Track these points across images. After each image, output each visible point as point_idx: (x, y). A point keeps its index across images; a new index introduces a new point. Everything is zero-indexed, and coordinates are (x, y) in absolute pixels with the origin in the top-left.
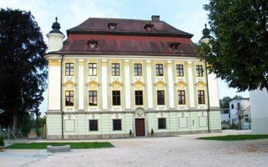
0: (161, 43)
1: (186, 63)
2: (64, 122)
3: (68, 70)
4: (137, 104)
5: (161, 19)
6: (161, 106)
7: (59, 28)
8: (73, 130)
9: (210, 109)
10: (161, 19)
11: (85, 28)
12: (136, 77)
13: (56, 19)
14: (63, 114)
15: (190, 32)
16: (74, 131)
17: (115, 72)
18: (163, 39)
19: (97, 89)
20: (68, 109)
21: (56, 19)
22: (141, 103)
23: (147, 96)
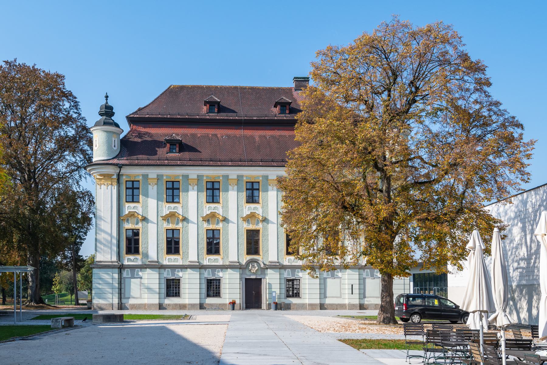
2: (122, 280)
6: (172, 257)
7: (113, 114)
8: (339, 296)
11: (157, 113)
12: (168, 205)
13: (107, 97)
14: (121, 268)
20: (129, 260)
22: (257, 252)
23: (147, 238)
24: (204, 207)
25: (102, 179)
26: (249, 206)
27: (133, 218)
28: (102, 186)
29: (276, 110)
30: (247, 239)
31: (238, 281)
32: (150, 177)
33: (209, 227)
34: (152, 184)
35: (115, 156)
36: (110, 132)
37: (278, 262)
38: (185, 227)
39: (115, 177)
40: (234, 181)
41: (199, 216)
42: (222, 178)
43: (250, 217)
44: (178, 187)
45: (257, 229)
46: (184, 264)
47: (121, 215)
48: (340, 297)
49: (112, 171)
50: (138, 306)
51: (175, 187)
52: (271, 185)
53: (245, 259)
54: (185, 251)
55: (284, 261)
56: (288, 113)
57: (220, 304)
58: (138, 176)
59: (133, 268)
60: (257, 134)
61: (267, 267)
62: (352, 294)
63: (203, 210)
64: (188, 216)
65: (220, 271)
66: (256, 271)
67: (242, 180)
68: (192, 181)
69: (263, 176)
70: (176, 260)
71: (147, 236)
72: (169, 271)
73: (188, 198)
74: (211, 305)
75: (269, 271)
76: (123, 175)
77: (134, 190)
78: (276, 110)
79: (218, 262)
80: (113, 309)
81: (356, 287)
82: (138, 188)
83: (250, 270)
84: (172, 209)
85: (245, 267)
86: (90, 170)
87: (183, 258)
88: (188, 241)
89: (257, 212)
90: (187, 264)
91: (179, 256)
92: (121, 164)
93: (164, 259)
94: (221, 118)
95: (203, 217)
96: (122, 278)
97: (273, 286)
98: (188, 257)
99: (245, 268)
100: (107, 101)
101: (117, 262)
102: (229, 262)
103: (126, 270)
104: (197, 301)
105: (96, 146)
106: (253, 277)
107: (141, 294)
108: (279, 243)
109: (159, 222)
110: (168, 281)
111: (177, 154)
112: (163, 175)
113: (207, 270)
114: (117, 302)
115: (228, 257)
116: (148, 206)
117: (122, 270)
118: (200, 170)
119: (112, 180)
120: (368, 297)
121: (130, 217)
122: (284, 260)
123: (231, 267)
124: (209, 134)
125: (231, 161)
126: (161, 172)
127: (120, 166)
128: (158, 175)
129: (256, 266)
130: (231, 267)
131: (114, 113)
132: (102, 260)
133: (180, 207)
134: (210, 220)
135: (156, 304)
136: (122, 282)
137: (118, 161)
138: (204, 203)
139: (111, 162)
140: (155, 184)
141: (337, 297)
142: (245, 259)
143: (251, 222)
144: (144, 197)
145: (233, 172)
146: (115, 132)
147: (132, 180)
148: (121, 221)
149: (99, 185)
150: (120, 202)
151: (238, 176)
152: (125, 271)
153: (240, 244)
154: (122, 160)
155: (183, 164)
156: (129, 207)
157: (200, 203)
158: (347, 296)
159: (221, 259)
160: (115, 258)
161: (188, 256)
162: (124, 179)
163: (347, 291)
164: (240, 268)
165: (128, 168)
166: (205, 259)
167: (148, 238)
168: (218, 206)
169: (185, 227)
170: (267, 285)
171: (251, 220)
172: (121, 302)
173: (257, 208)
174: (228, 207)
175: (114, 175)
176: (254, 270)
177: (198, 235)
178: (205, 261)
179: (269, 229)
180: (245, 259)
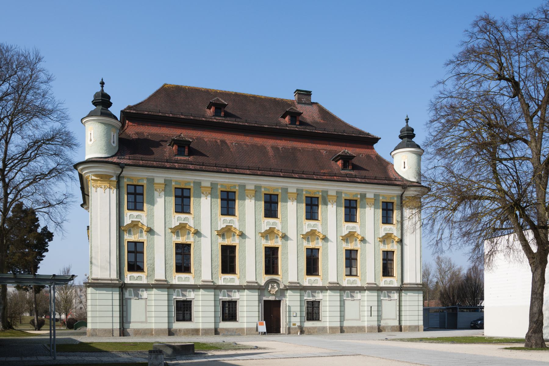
0: (272, 147)
1: (151, 181)
2: (124, 301)
4: (267, 272)
5: (313, 99)
6: (228, 276)
7: (110, 104)
10: (313, 99)
13: (102, 84)
14: (122, 287)
15: (374, 133)
16: (146, 322)
17: (135, 201)
18: (324, 148)
19: (144, 238)
21: (102, 84)
24: (219, 220)
25: (98, 180)
26: (267, 221)
27: (136, 229)
28: (99, 189)
29: (210, 112)
30: (190, 255)
31: (256, 303)
32: (247, 187)
33: (224, 242)
34: (158, 190)
35: (114, 154)
36: (109, 124)
37: (257, 283)
38: (197, 241)
39: (114, 179)
40: (251, 192)
41: (213, 230)
42: (238, 188)
43: (269, 233)
44: (141, 192)
45: (188, 243)
46: (196, 283)
47: (121, 225)
48: (360, 320)
49: (110, 171)
50: (143, 332)
51: (137, 192)
52: (291, 198)
53: (263, 279)
54: (198, 269)
55: (305, 281)
56: (298, 124)
57: (237, 329)
58: (142, 179)
59: (137, 287)
60: (269, 143)
61: (286, 289)
62: (371, 316)
63: (217, 223)
64: (201, 229)
65: (320, 292)
66: (277, 292)
67: (260, 192)
68: (292, 195)
69: (282, 189)
70: (138, 278)
71: (153, 250)
72: (225, 292)
73: (200, 209)
74: (227, 330)
75: (289, 293)
76: (123, 177)
77: (184, 199)
78: (210, 112)
79: (234, 282)
80: (113, 336)
81: (375, 309)
82: (142, 194)
83: (270, 291)
84: (182, 221)
85: (264, 288)
86: (82, 170)
87: (147, 276)
88: (201, 257)
89: (234, 226)
90: (200, 284)
91: (143, 273)
92: (122, 164)
93: (174, 277)
94: (230, 122)
95: (171, 229)
96: (124, 299)
97: (293, 309)
98: (200, 276)
99: (264, 289)
100: (103, 88)
101: (117, 280)
102: (247, 282)
103: (128, 289)
104: (212, 326)
105: (91, 140)
106: (272, 298)
107: (146, 317)
108: (299, 262)
109: (377, 244)
110: (224, 303)
111: (187, 158)
112: (171, 180)
113: (223, 290)
114: (118, 327)
115: (245, 277)
116: (153, 216)
117: (124, 289)
118: (240, 178)
119: (111, 183)
120: (385, 319)
121: (133, 227)
122: (304, 280)
123: (250, 287)
124: (217, 139)
125: (249, 170)
126: (217, 180)
127: (122, 166)
128: (165, 180)
129: (276, 286)
130: (250, 287)
131: (112, 103)
132: (99, 277)
133: (192, 219)
134: (225, 234)
135: (165, 330)
136: (124, 304)
137: (119, 160)
138: (219, 215)
139: (110, 160)
140: (163, 190)
141: (142, 322)
142: (263, 279)
143: (270, 238)
144: (149, 205)
145: (332, 188)
146: (114, 126)
147: (135, 183)
148: (121, 231)
149: (94, 187)
150: (121, 209)
151: (256, 187)
152: (128, 291)
153: (258, 262)
154: (123, 159)
155: (370, 182)
156: (132, 215)
157: (214, 215)
158: (366, 319)
159: (237, 279)
160: (114, 276)
161: (201, 275)
162: (125, 182)
163: (366, 314)
164: (259, 289)
165: (130, 169)
166: (220, 278)
167: (154, 253)
168: (317, 224)
169: (197, 241)
170: (288, 307)
171: (270, 237)
172: (123, 327)
173: (277, 223)
174: (245, 220)
175: (113, 176)
176: (273, 291)
177: (212, 251)
178: (220, 280)
179: (289, 247)
180: (263, 279)
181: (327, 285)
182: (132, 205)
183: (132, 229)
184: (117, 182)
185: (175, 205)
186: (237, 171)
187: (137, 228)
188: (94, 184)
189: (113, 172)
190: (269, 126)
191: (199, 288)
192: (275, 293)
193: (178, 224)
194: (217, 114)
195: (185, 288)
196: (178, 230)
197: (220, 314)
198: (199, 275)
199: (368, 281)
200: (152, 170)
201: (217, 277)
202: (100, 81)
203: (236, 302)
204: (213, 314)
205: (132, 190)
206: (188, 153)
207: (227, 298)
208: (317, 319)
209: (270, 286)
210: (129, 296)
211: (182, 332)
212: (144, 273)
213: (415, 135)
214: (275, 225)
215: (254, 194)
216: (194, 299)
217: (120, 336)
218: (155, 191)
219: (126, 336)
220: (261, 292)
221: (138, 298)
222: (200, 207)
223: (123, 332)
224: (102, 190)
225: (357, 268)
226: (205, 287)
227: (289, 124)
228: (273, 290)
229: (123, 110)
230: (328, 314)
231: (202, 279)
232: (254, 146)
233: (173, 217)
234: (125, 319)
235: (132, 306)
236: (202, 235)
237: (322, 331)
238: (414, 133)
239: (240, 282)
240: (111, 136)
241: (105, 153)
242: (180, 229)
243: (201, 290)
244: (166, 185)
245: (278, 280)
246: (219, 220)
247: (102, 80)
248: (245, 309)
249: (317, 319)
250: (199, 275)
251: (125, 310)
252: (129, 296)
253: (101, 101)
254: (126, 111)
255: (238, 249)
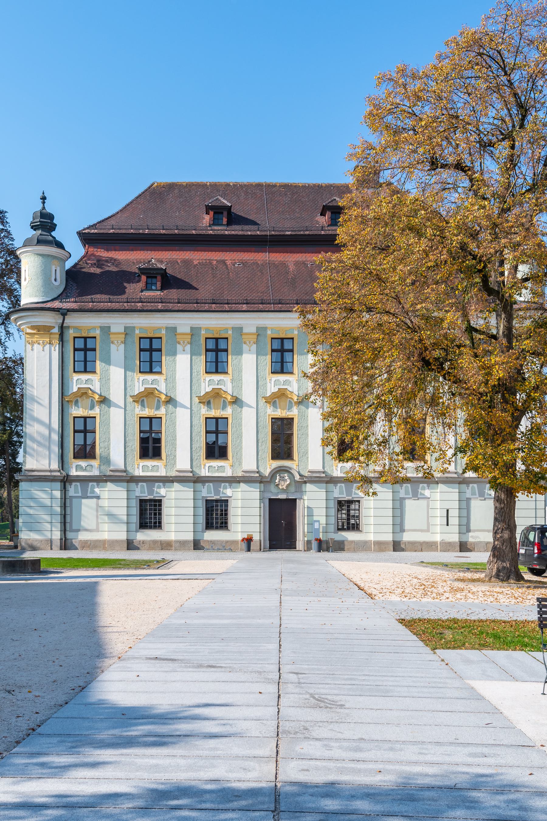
2: (68, 501)
3: (80, 355)
4: (276, 456)
6: (216, 463)
7: (53, 227)
9: (58, 485)
13: (44, 198)
19: (228, 412)
20: (78, 468)
21: (44, 198)
22: (289, 456)
24: (202, 380)
25: (34, 334)
27: (85, 398)
32: (113, 330)
33: (210, 413)
35: (56, 296)
36: (48, 256)
37: (324, 472)
38: (170, 413)
39: (56, 330)
40: (251, 336)
41: (194, 396)
44: (225, 347)
46: (168, 475)
48: (428, 530)
49: (50, 320)
57: (227, 542)
59: (84, 480)
62: (447, 525)
63: (200, 385)
64: (175, 395)
65: (228, 487)
66: (288, 486)
67: (265, 336)
70: (155, 468)
74: (212, 542)
75: (309, 487)
76: (68, 327)
77: (153, 353)
79: (224, 472)
80: (51, 549)
81: (455, 513)
83: (278, 485)
84: (148, 384)
85: (269, 480)
89: (290, 389)
91: (160, 461)
93: (136, 466)
94: (233, 233)
95: (199, 397)
96: (67, 497)
97: (316, 512)
100: (44, 205)
101: (59, 471)
103: (74, 484)
104: (190, 537)
105: (55, 280)
111: (159, 293)
113: (207, 484)
115: (240, 464)
116: (109, 379)
117: (67, 484)
119: (52, 336)
120: (475, 531)
122: (334, 468)
123: (247, 479)
127: (64, 313)
129: (286, 478)
130: (247, 479)
134: (212, 401)
135: (122, 541)
136: (68, 504)
139: (49, 305)
140: (122, 342)
141: (422, 531)
142: (268, 466)
143: (280, 404)
144: (104, 364)
147: (84, 335)
149: (29, 343)
152: (73, 486)
153: (260, 441)
155: (166, 308)
156: (80, 380)
158: (438, 529)
160: (55, 466)
161: (175, 462)
164: (261, 482)
166: (202, 466)
168: (225, 379)
170: (306, 509)
172: (65, 538)
173: (290, 382)
175: (54, 327)
176: (283, 485)
178: (203, 470)
181: (174, 474)
182: (80, 366)
183: (79, 399)
184: (60, 335)
185: (161, 362)
186: (228, 307)
187: (86, 398)
188: (29, 339)
189: (54, 321)
190: (293, 233)
191: (172, 481)
192: (285, 488)
193: (143, 390)
194: (215, 222)
195: (151, 481)
196: (143, 398)
197: (202, 519)
198: (173, 461)
199: (311, 467)
200: (105, 315)
201: (199, 465)
202: (41, 195)
203: (160, 501)
204: (191, 519)
205: (80, 344)
206: (162, 286)
207: (213, 496)
208: (158, 525)
209: (278, 478)
210: (75, 493)
211: (147, 546)
212: (162, 461)
213: (56, 225)
214: (288, 385)
215: (190, 340)
216: (164, 497)
217: (61, 549)
218: (111, 344)
219: (69, 549)
220: (264, 486)
221: (483, 499)
222: (175, 363)
223: (65, 545)
224: (40, 347)
225: (74, 445)
226: (181, 480)
227: (329, 226)
228: (282, 483)
229: (80, 231)
230: (372, 521)
231: (309, 468)
232: (272, 264)
233: (136, 380)
234: (68, 526)
235: (406, 509)
236: (178, 403)
237: (364, 546)
238: (54, 222)
239: (233, 472)
240: (51, 271)
241: (43, 296)
242: (146, 396)
243: (175, 483)
244: (126, 334)
245: (290, 468)
246: (202, 380)
247: (43, 193)
248: (239, 512)
249: (158, 525)
250: (173, 461)
251: (69, 513)
252: (75, 493)
253: (39, 223)
254: (84, 232)
255: (297, 422)
